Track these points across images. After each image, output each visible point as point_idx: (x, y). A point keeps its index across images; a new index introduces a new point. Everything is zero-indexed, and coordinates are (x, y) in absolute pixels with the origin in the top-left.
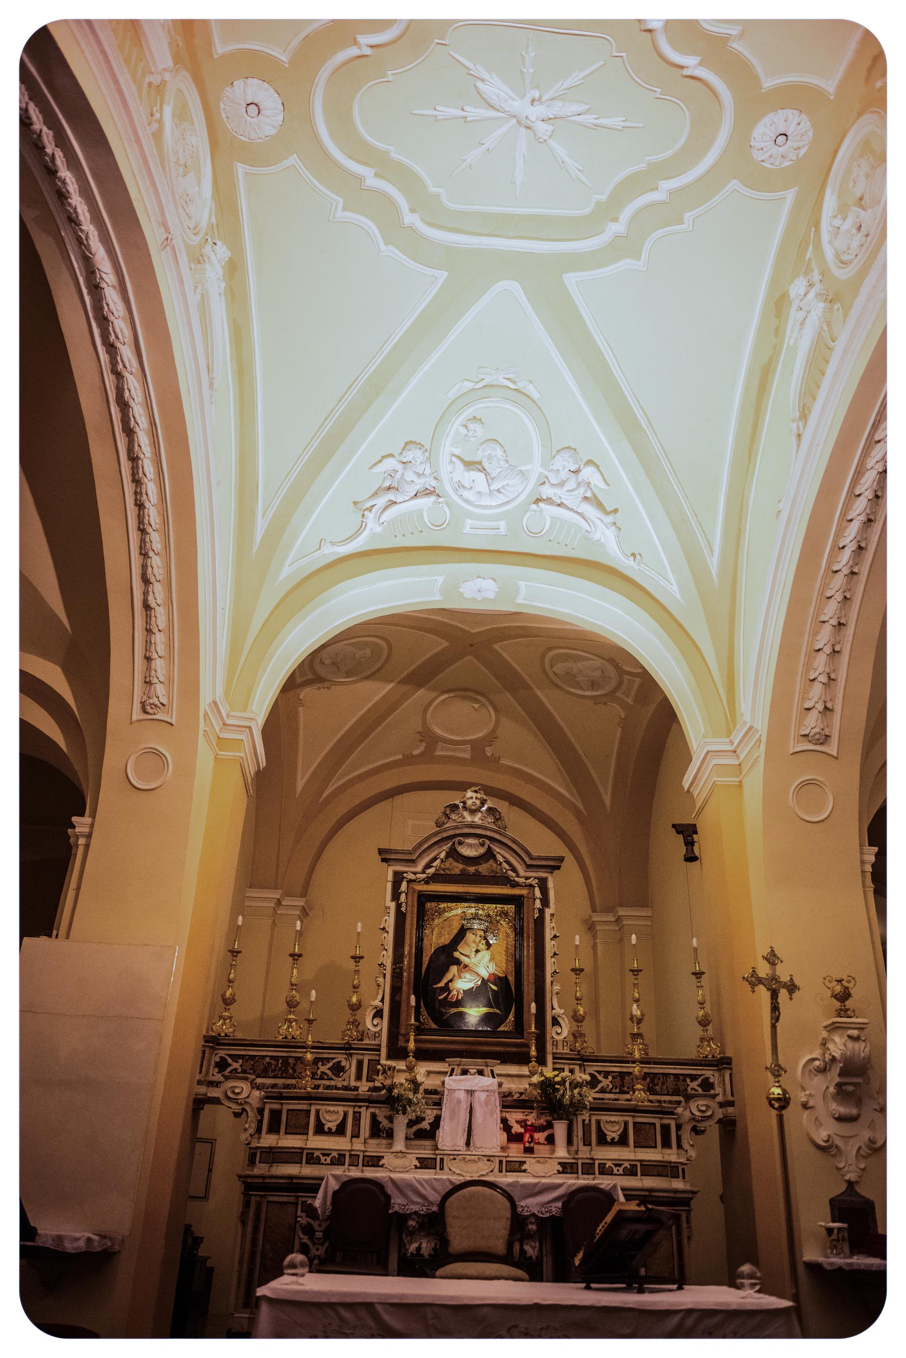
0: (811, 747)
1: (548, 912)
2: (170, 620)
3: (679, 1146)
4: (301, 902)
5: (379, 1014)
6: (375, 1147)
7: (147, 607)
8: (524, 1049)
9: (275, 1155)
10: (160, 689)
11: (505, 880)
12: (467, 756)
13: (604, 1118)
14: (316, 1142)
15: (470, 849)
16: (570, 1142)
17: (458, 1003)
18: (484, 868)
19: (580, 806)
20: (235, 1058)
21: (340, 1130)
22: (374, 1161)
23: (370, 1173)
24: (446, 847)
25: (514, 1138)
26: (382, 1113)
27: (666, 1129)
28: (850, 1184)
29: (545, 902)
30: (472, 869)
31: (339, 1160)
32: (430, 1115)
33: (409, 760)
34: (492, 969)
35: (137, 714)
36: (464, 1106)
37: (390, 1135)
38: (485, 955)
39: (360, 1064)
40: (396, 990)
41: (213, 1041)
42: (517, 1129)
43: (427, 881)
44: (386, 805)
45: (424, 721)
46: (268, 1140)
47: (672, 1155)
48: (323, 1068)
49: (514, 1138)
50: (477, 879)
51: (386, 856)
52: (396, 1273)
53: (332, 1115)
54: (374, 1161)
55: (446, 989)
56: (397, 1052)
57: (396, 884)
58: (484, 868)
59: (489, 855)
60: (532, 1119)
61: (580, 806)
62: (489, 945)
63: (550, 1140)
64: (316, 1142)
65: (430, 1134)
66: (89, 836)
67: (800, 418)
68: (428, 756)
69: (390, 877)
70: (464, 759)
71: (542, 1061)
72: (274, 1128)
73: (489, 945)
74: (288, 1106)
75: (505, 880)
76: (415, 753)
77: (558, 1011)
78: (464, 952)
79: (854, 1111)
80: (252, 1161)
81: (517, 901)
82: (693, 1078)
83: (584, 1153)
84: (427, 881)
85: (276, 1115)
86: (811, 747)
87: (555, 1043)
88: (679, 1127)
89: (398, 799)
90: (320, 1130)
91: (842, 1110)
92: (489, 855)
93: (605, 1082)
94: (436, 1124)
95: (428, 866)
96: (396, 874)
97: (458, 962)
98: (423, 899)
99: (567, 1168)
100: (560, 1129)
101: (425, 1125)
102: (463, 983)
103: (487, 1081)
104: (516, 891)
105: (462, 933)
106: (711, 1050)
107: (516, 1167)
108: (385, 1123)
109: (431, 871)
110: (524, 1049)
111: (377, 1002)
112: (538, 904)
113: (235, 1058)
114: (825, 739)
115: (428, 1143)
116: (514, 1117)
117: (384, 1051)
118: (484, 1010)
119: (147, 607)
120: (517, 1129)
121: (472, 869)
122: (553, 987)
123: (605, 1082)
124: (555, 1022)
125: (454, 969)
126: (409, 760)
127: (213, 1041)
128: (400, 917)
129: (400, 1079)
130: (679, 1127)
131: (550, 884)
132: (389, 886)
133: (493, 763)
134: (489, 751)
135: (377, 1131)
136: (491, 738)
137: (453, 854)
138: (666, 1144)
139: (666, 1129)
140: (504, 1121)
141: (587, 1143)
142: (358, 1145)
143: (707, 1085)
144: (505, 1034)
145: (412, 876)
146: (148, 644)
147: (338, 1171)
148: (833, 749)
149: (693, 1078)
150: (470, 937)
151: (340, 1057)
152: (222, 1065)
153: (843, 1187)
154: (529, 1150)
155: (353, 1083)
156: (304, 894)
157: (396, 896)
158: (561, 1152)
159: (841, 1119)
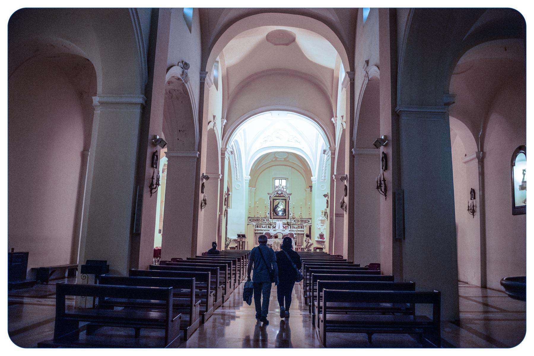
0: (323, 181)
1: (290, 201)
2: (239, 169)
3: (303, 228)
4: (255, 188)
5: (269, 214)
6: (269, 229)
7: (236, 167)
8: (212, 276)
9: (258, 230)
10: (238, 177)
11: (284, 197)
12: (283, 160)
13: (294, 225)
14: (262, 229)
15: (280, 192)
16: (290, 228)
17: (278, 212)
18: (281, 195)
19: (304, 168)
20: (252, 219)
21: (265, 227)
22: (269, 230)
23: (268, 232)
24: (276, 192)
25: (284, 228)
26: (269, 225)
27: (302, 227)
28: (322, 232)
29: (289, 199)
30: (280, 195)
31: (265, 230)
32: (275, 225)
33: (272, 161)
34: (283, 207)
35: (236, 180)
36: (279, 225)
37: (270, 228)
38: (282, 206)
39: (267, 220)
40: (270, 211)
41: (249, 217)
42: (285, 227)
43: (274, 197)
44: (269, 168)
45: (275, 155)
46: (257, 229)
47: (302, 229)
48: (262, 220)
49: (284, 228)
50: (281, 196)
51: (268, 194)
52: (160, 9)
53: (264, 226)
54: (269, 230)
55: (277, 210)
56: (271, 218)
57: (270, 198)
58: (281, 195)
59: (282, 193)
60: (286, 226)
61: (304, 168)
62: (282, 205)
63: (288, 228)
64: (262, 229)
65: (275, 227)
66: (232, 195)
67: (213, 327)
68: (276, 160)
69: (269, 197)
70: (283, 161)
71: (288, 219)
72: (257, 227)
73: (282, 205)
74: (259, 225)
75: (284, 197)
76: (273, 160)
77: (291, 213)
78: (279, 205)
79: (323, 225)
80: (255, 231)
81: (286, 199)
82: (307, 220)
83: (292, 229)
84: (274, 197)
85: (258, 226)
86: (323, 181)
87: (290, 217)
88: (303, 226)
89: (271, 168)
90: (263, 227)
91: (322, 225)
92: (282, 193)
93: (296, 221)
94: (275, 227)
95: (274, 195)
96: (270, 196)
97: (278, 207)
98: (274, 200)
99: (290, 231)
100: (289, 227)
101: (274, 227)
102: (279, 209)
103: (281, 222)
104: (286, 198)
105: (279, 203)
106: (310, 217)
107: (284, 231)
108: (270, 227)
109: (274, 196)
110: (212, 276)
111: (268, 212)
112: (288, 200)
113: (252, 219)
114: (325, 180)
115: (275, 228)
116: (284, 226)
117: (269, 218)
118: (282, 213)
119: (236, 167)
120: (285, 227)
121: (280, 195)
122: (290, 210)
123: (296, 221)
124: (290, 214)
125: (278, 208)
126: (272, 161)
127: (249, 217)
128: (271, 202)
129: (271, 221)
130: (303, 226)
131: (290, 197)
132: (269, 198)
133: (288, 161)
134: (287, 159)
135: (269, 227)
136: (287, 157)
137: (277, 193)
138: (302, 228)
139: (302, 227)
140: (283, 226)
141: (292, 228)
142: (267, 229)
143: (309, 221)
144: (284, 216)
145: (272, 196)
146: (236, 172)
147: (265, 231)
148: (326, 181)
149: (307, 220)
150: (280, 203)
151: (264, 219)
152: (250, 220)
153: (321, 233)
154: (286, 229)
155: (266, 222)
156: (255, 187)
157: (270, 199)
158: (289, 229)
159: (321, 226)
